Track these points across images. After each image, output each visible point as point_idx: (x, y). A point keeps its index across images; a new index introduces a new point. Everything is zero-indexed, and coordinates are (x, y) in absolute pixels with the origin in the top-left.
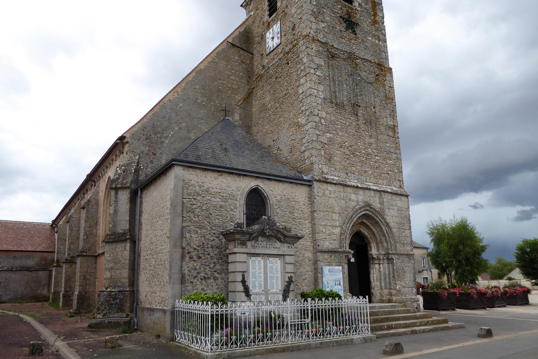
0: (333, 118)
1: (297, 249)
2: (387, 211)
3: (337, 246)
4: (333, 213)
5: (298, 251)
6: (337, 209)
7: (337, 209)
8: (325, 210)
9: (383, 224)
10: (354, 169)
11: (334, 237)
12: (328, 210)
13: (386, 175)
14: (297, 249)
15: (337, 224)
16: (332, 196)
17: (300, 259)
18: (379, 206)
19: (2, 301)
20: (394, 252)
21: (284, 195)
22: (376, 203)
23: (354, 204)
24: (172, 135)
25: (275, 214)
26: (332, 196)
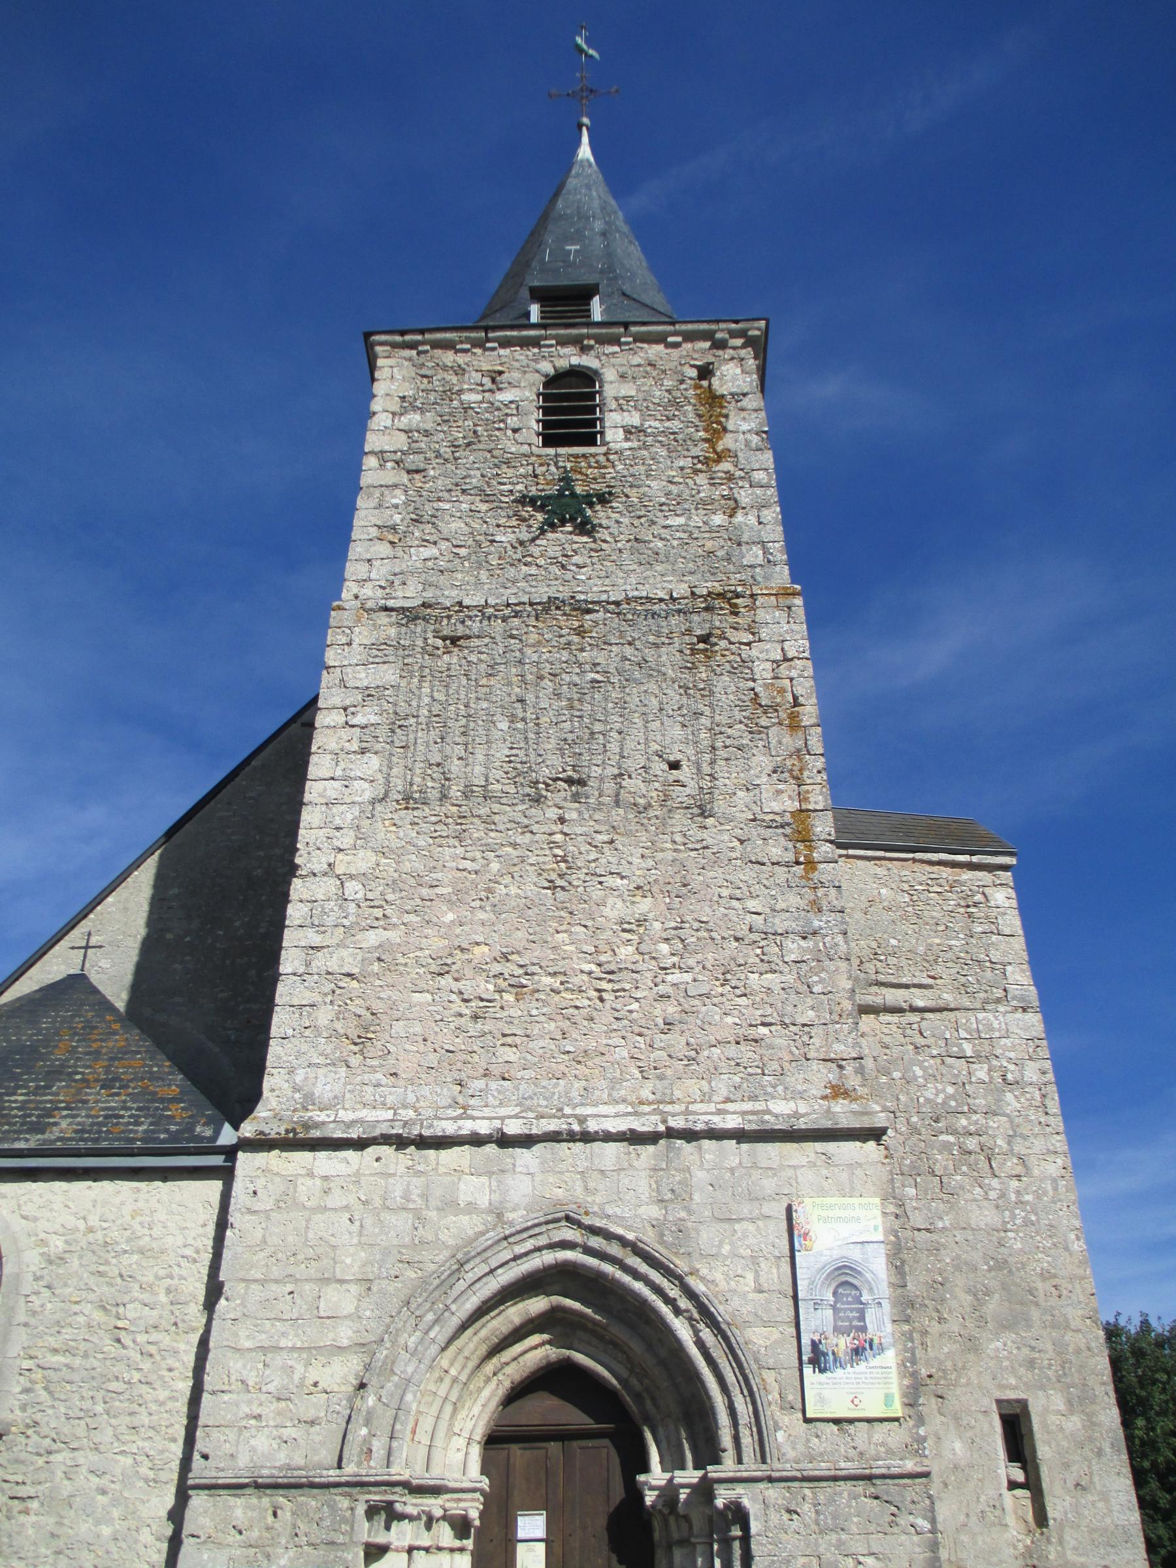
0: (412, 863)
1: (104, 1482)
2: (707, 1236)
3: (327, 1456)
4: (326, 1281)
5: (104, 1492)
6: (351, 1262)
7: (351, 1262)
8: (276, 1272)
9: (677, 1312)
10: (510, 1054)
11: (313, 1406)
12: (300, 1271)
13: (732, 1050)
14: (104, 1482)
15: (345, 1334)
16: (336, 1199)
17: (106, 1531)
18: (655, 1212)
19: (922, 1556)
20: (751, 1467)
21: (91, 1230)
22: (624, 1196)
23: (469, 1224)
24: (922, 1077)
25: (22, 1317)
26: (336, 1199)
